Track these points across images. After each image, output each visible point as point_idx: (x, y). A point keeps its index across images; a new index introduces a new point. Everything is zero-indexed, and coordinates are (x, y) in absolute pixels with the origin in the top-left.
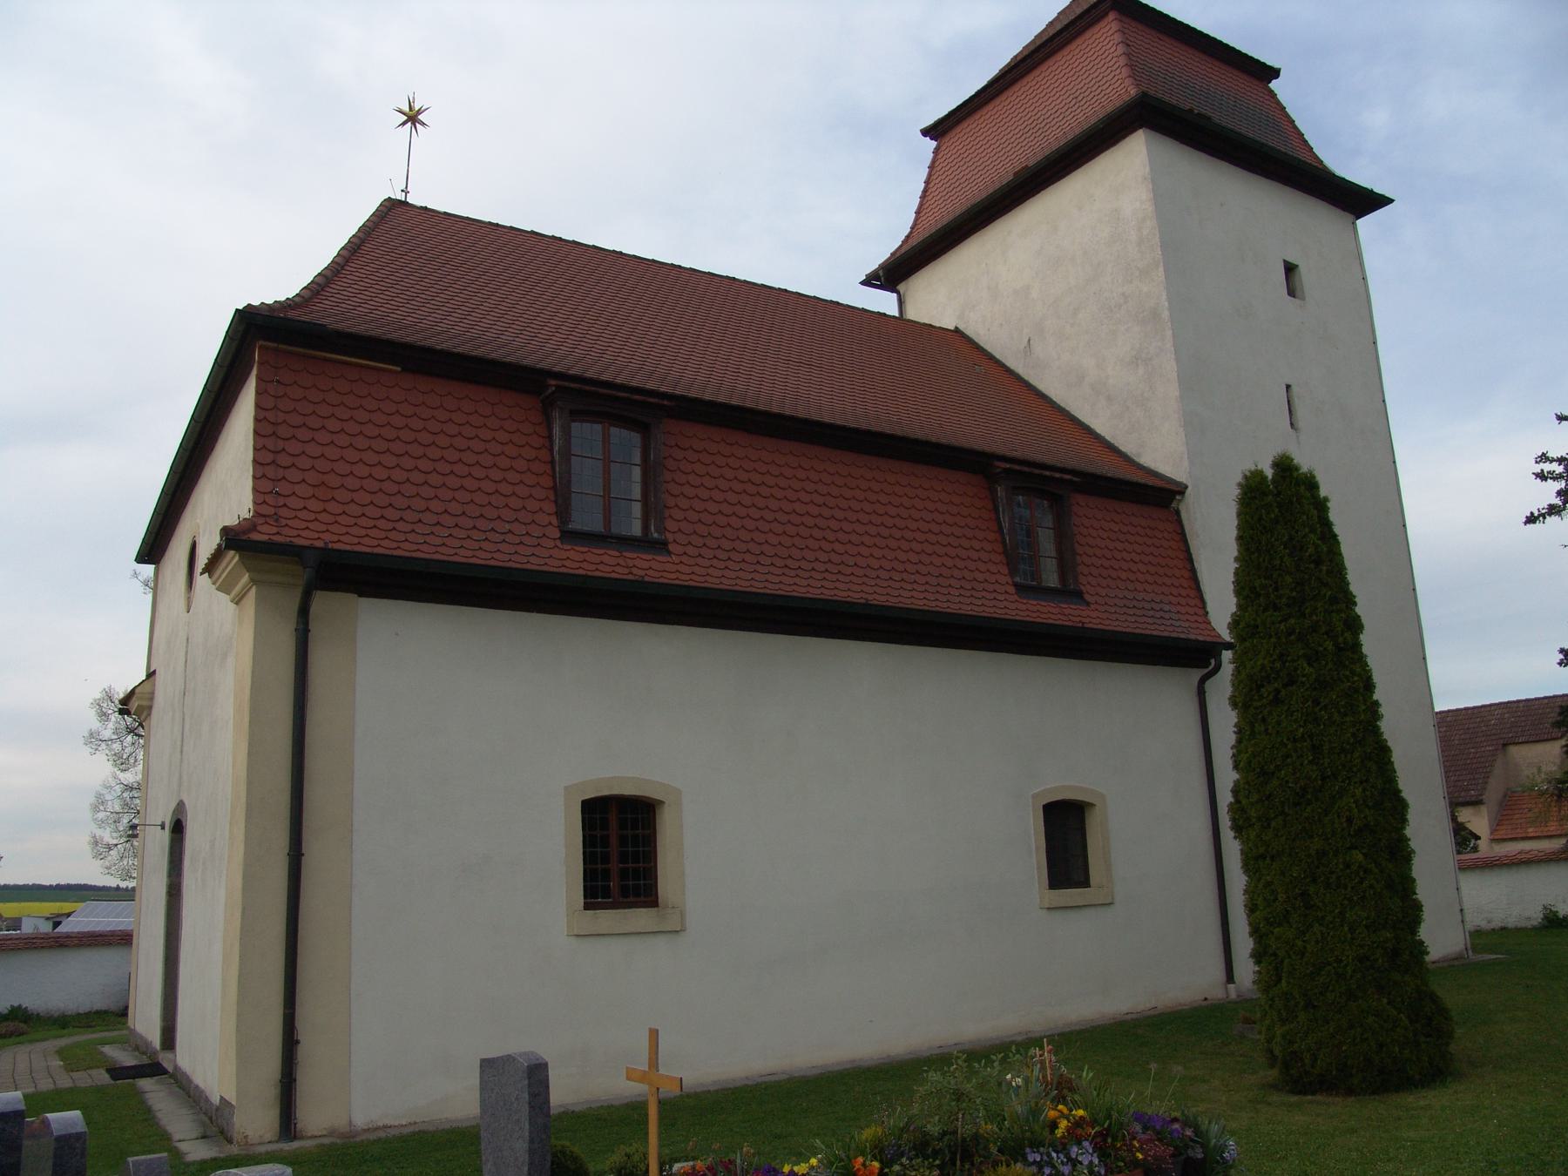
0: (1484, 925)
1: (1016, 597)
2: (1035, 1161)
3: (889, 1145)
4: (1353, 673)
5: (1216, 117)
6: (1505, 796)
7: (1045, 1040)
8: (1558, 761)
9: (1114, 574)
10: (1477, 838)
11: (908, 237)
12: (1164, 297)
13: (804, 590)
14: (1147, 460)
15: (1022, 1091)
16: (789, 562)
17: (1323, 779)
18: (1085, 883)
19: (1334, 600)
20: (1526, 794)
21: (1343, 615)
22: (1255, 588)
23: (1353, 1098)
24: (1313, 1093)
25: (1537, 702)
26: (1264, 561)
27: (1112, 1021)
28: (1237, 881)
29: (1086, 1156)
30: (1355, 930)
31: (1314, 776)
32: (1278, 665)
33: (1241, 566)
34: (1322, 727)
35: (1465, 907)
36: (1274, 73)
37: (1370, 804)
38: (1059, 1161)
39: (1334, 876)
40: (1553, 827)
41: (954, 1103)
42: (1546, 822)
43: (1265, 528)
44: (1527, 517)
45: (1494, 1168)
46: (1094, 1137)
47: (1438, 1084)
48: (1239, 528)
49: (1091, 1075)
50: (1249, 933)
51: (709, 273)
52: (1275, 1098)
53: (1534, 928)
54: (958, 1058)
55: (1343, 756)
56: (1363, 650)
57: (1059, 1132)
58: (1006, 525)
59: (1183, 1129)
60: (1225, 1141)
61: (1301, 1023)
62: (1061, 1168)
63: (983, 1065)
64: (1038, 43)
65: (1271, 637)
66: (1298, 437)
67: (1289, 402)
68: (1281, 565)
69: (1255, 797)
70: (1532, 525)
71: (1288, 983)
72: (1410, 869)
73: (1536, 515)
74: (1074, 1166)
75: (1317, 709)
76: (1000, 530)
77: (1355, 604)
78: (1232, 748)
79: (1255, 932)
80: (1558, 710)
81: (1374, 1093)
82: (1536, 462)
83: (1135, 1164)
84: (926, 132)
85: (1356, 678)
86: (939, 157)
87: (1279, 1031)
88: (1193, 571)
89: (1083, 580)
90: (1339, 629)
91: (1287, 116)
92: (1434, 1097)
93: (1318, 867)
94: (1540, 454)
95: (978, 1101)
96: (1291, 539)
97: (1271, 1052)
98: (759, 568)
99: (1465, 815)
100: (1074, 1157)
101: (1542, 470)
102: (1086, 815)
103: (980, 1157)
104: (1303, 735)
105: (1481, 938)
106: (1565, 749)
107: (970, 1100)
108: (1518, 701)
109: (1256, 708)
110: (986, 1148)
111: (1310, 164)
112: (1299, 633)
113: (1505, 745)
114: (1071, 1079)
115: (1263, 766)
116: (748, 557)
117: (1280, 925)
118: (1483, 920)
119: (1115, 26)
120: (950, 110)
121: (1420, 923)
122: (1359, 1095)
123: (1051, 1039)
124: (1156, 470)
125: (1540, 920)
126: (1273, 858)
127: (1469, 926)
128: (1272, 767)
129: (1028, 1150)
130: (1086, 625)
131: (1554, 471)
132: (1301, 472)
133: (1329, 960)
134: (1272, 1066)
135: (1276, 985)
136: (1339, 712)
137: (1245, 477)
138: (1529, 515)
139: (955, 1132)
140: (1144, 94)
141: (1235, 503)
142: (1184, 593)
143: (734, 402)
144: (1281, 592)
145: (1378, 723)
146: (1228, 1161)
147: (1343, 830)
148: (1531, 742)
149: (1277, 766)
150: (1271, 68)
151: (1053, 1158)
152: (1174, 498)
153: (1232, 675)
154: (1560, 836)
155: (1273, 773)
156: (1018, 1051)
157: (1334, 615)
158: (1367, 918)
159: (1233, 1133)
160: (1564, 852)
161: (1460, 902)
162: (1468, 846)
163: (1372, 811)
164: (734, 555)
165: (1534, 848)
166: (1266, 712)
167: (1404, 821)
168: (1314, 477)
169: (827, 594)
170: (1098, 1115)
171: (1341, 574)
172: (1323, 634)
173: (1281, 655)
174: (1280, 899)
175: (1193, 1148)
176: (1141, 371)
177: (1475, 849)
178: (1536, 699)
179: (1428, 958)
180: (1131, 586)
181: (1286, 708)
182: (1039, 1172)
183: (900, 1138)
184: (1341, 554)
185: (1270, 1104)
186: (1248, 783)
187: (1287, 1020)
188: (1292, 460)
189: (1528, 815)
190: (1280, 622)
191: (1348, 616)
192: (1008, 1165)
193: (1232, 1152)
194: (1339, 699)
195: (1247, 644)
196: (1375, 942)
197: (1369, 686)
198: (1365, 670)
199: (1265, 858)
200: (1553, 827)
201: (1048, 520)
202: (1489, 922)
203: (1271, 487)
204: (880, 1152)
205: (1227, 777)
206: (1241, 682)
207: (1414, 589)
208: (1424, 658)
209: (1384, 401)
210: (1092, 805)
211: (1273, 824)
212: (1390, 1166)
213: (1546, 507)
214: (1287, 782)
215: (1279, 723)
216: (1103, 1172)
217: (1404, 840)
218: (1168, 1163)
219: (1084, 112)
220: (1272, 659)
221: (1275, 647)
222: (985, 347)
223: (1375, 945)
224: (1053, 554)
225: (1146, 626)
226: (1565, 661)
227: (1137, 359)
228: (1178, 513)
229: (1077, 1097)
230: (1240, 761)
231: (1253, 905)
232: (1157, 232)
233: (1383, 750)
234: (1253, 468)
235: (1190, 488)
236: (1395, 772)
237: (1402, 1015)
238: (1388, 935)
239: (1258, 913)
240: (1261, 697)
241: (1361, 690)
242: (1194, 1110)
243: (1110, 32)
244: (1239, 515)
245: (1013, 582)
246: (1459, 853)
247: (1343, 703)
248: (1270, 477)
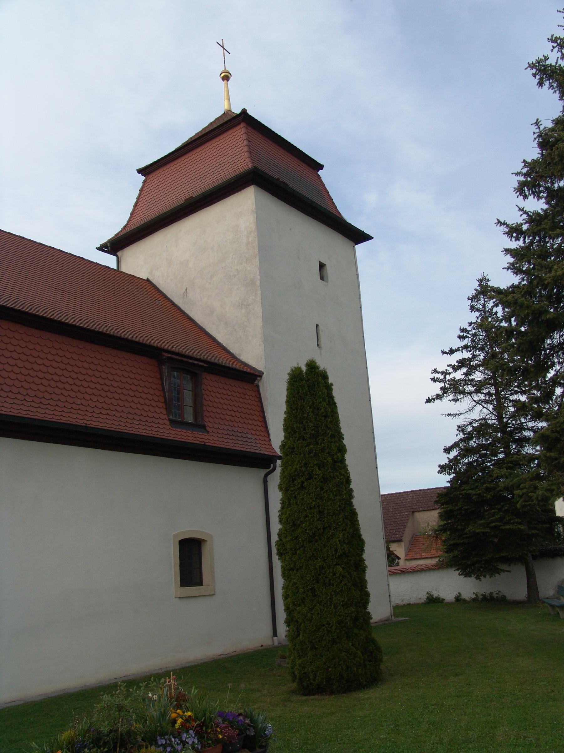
0: (400, 603)
1: (170, 427)
2: (162, 744)
3: (77, 742)
4: (340, 474)
5: (291, 185)
6: (412, 537)
7: (172, 673)
8: (437, 520)
9: (223, 417)
10: (399, 558)
11: (125, 227)
12: (258, 273)
13: (51, 417)
14: (244, 358)
15: (156, 703)
16: (43, 401)
17: (324, 528)
18: (200, 583)
19: (333, 436)
20: (422, 536)
21: (337, 444)
22: (294, 428)
23: (334, 696)
24: (314, 695)
25: (389, 496)
26: (299, 414)
27: (212, 659)
28: (279, 582)
29: (191, 738)
30: (337, 607)
31: (319, 527)
32: (303, 469)
33: (287, 417)
34: (324, 501)
35: (392, 593)
36: (321, 167)
37: (347, 542)
38: (176, 743)
39: (327, 579)
40: (433, 553)
41: (117, 713)
42: (430, 550)
43: (300, 397)
44: (427, 399)
45: (397, 728)
46: (196, 727)
47: (374, 686)
48: (288, 396)
49: (196, 691)
50: (284, 610)
51: (9, 233)
52: (295, 698)
53: (423, 603)
54: (121, 686)
55: (334, 517)
56: (346, 463)
57: (177, 726)
58: (166, 387)
59: (244, 719)
60: (266, 725)
61: (309, 657)
62: (176, 747)
63: (134, 689)
64: (204, 133)
65: (300, 454)
66: (320, 351)
67: (317, 333)
68: (307, 417)
69: (289, 538)
70: (429, 404)
71: (303, 636)
72: (365, 576)
73: (431, 399)
74: (184, 745)
75: (322, 492)
76: (163, 390)
77: (343, 439)
78: (279, 512)
79: (287, 609)
80: (437, 495)
81: (343, 693)
82: (432, 373)
83: (218, 741)
84: (140, 171)
85: (342, 477)
86: (146, 185)
87: (298, 662)
88: (264, 417)
89: (206, 419)
90: (335, 451)
91: (326, 189)
92: (372, 693)
93: (320, 575)
94: (434, 369)
95: (131, 711)
96: (313, 404)
97: (294, 673)
98: (24, 402)
99: (394, 547)
100: (184, 740)
101: (434, 377)
102: (202, 545)
103: (131, 744)
104: (314, 506)
105: (398, 609)
106: (439, 514)
107: (126, 710)
108: (420, 490)
109: (292, 491)
110: (135, 739)
111: (335, 215)
112: (315, 452)
113: (413, 512)
114: (185, 694)
115: (294, 522)
116: (19, 396)
117: (300, 605)
118: (400, 600)
119: (244, 130)
120: (154, 161)
121: (368, 603)
122: (336, 694)
123: (175, 671)
124: (248, 363)
125: (425, 600)
126: (297, 570)
127: (393, 604)
128: (299, 522)
129: (158, 738)
130: (207, 444)
131: (439, 378)
132: (320, 369)
133: (324, 623)
134: (294, 681)
135: (297, 638)
136: (333, 494)
137: (292, 370)
138: (427, 398)
139: (117, 731)
140: (255, 167)
141: (286, 383)
142: (259, 429)
143: (17, 307)
144: (307, 431)
145: (352, 500)
146: (267, 736)
147: (333, 555)
148: (425, 511)
149: (301, 522)
150: (319, 164)
151: (172, 742)
152: (257, 379)
153: (280, 473)
154: (436, 557)
155: (299, 525)
156: (155, 680)
157: (333, 444)
158: (343, 601)
159: (272, 719)
160: (437, 566)
161: (389, 592)
162: (394, 562)
163: (347, 546)
164: (10, 395)
165: (424, 564)
166: (296, 493)
167: (362, 550)
168: (326, 373)
169: (64, 420)
170: (199, 714)
171: (337, 423)
172: (327, 453)
173: (306, 464)
174: (300, 592)
175: (249, 730)
176: (243, 311)
177: (398, 564)
178: (428, 489)
179: (372, 621)
180: (231, 424)
181: (307, 491)
182: (164, 751)
183: (85, 736)
184: (337, 413)
185: (292, 702)
186: (286, 530)
187: (302, 656)
188: (316, 363)
189: (422, 547)
190: (306, 446)
191: (339, 445)
192: (147, 748)
193: (270, 730)
194: (333, 488)
195: (289, 457)
196: (346, 614)
197: (348, 481)
198: (346, 473)
199: (294, 570)
200: (433, 553)
201: (190, 386)
202: (402, 601)
203: (305, 376)
204: (72, 747)
205: (276, 527)
206: (284, 477)
207: (373, 433)
208: (377, 468)
209: (363, 337)
210: (205, 541)
211: (298, 552)
212: (349, 732)
213: (435, 395)
214: (306, 530)
215: (303, 499)
216: (200, 748)
217: (362, 560)
218: (236, 739)
219: (224, 172)
220: (300, 466)
221: (302, 460)
222: (162, 290)
223: (347, 615)
224: (191, 405)
225: (238, 445)
226: (441, 471)
227: (242, 305)
228: (258, 386)
229: (188, 705)
230: (283, 519)
231: (287, 595)
232: (257, 239)
233: (353, 515)
234: (296, 366)
235: (264, 374)
236: (359, 525)
237: (358, 651)
238: (353, 610)
239: (289, 599)
240: (294, 485)
241: (344, 483)
242: (253, 707)
243: (241, 134)
244: (288, 390)
245: (169, 418)
246: (390, 566)
247: (335, 489)
248: (304, 371)
